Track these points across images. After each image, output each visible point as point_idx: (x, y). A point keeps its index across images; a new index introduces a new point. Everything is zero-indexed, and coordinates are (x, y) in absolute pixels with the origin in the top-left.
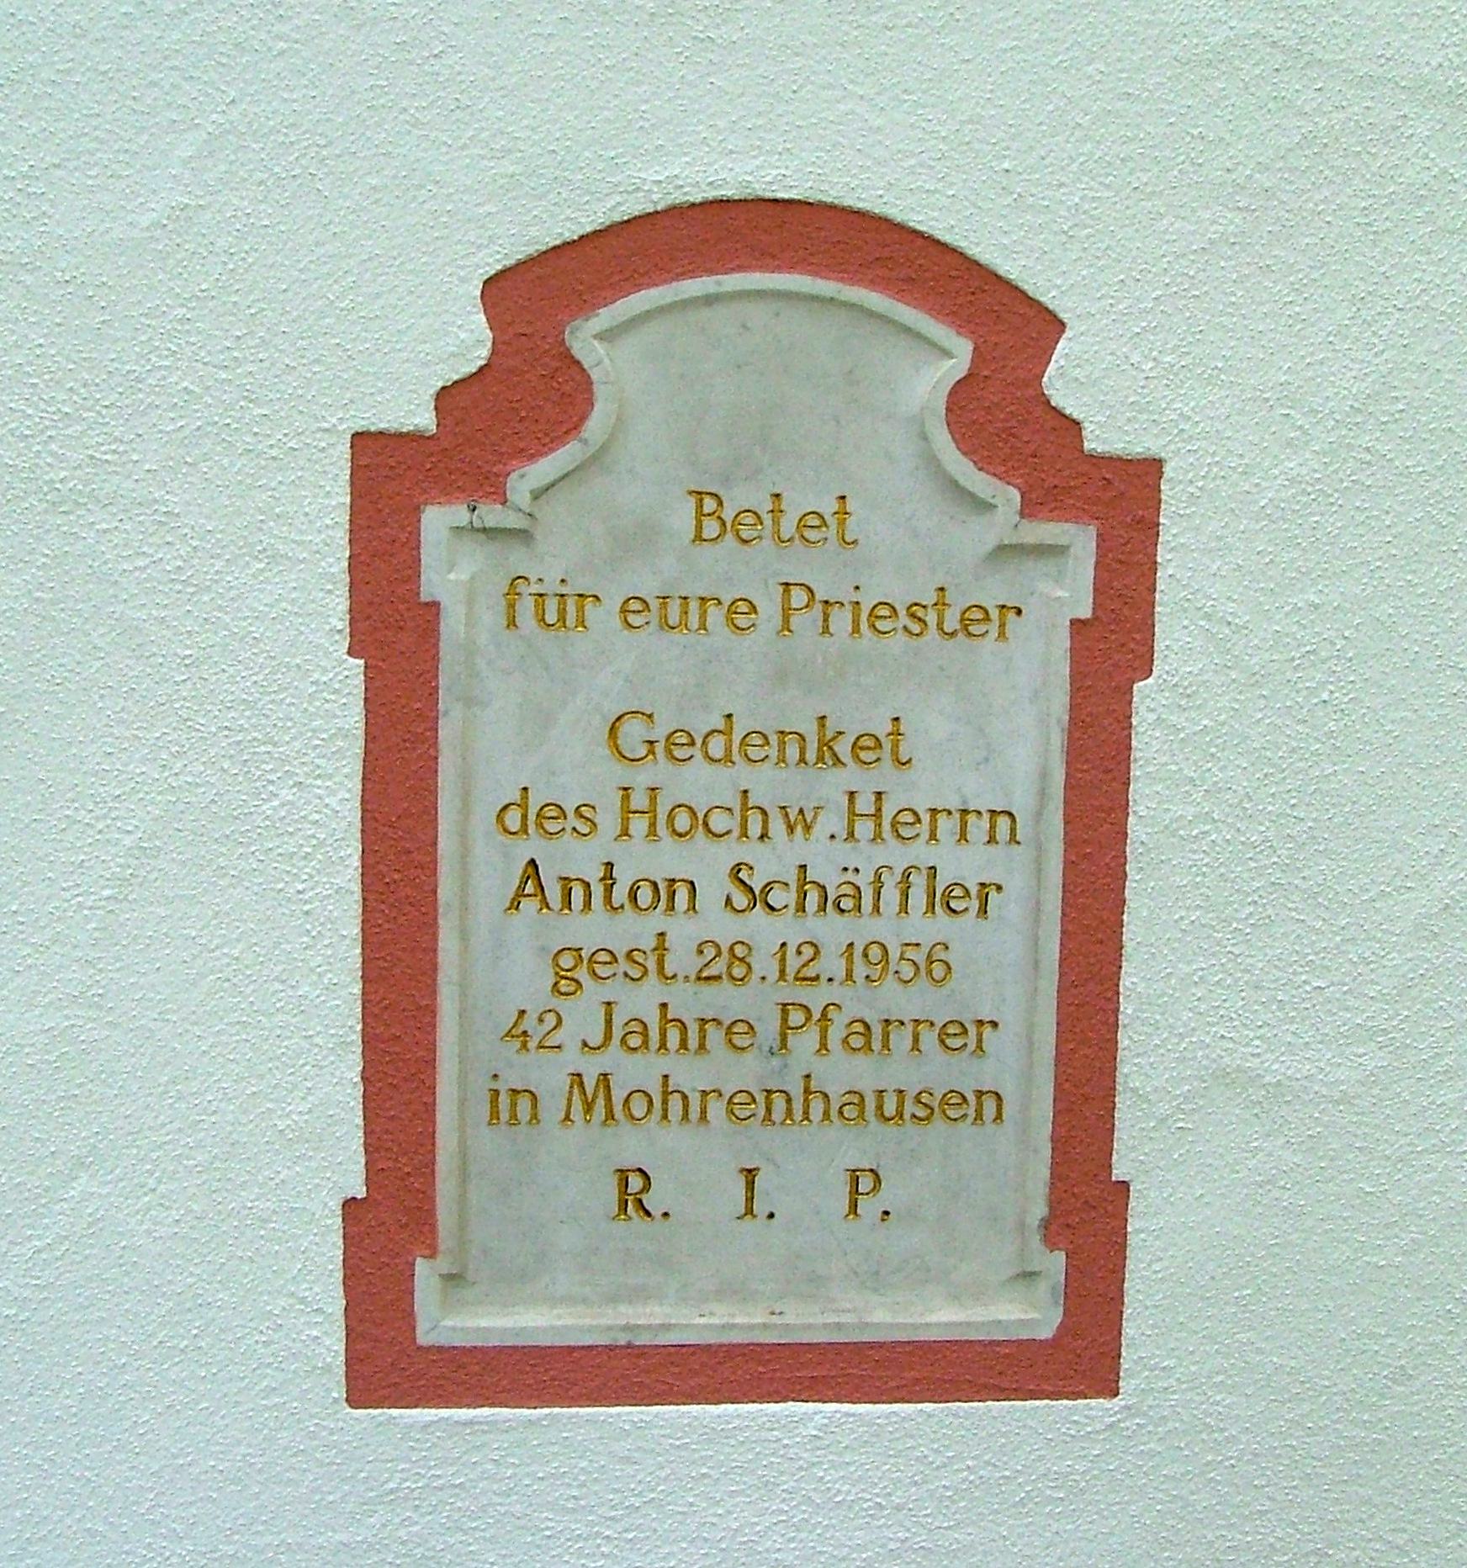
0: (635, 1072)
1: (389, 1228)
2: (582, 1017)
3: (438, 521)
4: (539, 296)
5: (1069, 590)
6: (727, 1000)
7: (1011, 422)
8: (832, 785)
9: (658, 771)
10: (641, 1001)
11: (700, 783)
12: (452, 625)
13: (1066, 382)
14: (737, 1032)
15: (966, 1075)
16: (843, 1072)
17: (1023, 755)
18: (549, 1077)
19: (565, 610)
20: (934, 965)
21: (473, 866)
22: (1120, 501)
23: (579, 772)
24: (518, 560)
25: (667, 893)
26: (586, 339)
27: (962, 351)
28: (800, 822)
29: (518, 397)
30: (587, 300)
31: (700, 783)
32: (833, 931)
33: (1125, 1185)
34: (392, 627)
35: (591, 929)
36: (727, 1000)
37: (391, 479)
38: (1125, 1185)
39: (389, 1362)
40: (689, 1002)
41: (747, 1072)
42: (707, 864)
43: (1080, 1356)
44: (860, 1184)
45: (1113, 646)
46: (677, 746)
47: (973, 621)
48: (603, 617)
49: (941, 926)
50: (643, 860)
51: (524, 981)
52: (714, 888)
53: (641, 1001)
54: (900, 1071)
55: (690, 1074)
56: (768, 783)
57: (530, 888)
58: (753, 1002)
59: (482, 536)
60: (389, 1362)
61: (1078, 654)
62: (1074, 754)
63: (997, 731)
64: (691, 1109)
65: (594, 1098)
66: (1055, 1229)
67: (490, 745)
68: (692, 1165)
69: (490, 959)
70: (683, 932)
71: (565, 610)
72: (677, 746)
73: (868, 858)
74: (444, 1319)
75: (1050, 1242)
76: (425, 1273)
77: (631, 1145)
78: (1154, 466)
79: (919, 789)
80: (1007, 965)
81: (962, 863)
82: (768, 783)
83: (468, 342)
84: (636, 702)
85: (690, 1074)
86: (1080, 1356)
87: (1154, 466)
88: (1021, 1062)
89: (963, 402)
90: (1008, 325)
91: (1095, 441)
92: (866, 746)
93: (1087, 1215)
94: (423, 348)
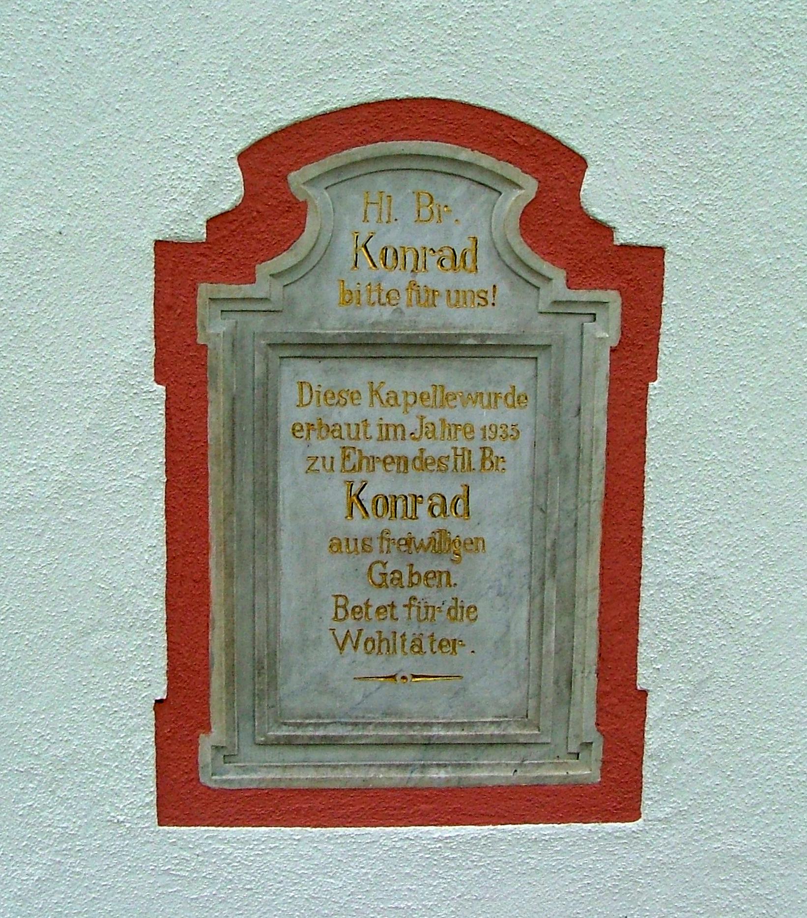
1: (179, 719)
4: (270, 159)
5: (606, 331)
26: (297, 180)
29: (258, 225)
33: (645, 693)
34: (179, 360)
35: (361, 427)
38: (645, 693)
39: (183, 798)
43: (616, 794)
59: (423, 747)
60: (183, 798)
74: (216, 774)
75: (158, 383)
78: (661, 250)
84: (351, 257)
86: (616, 794)
87: (661, 250)
89: (532, 222)
93: (622, 708)
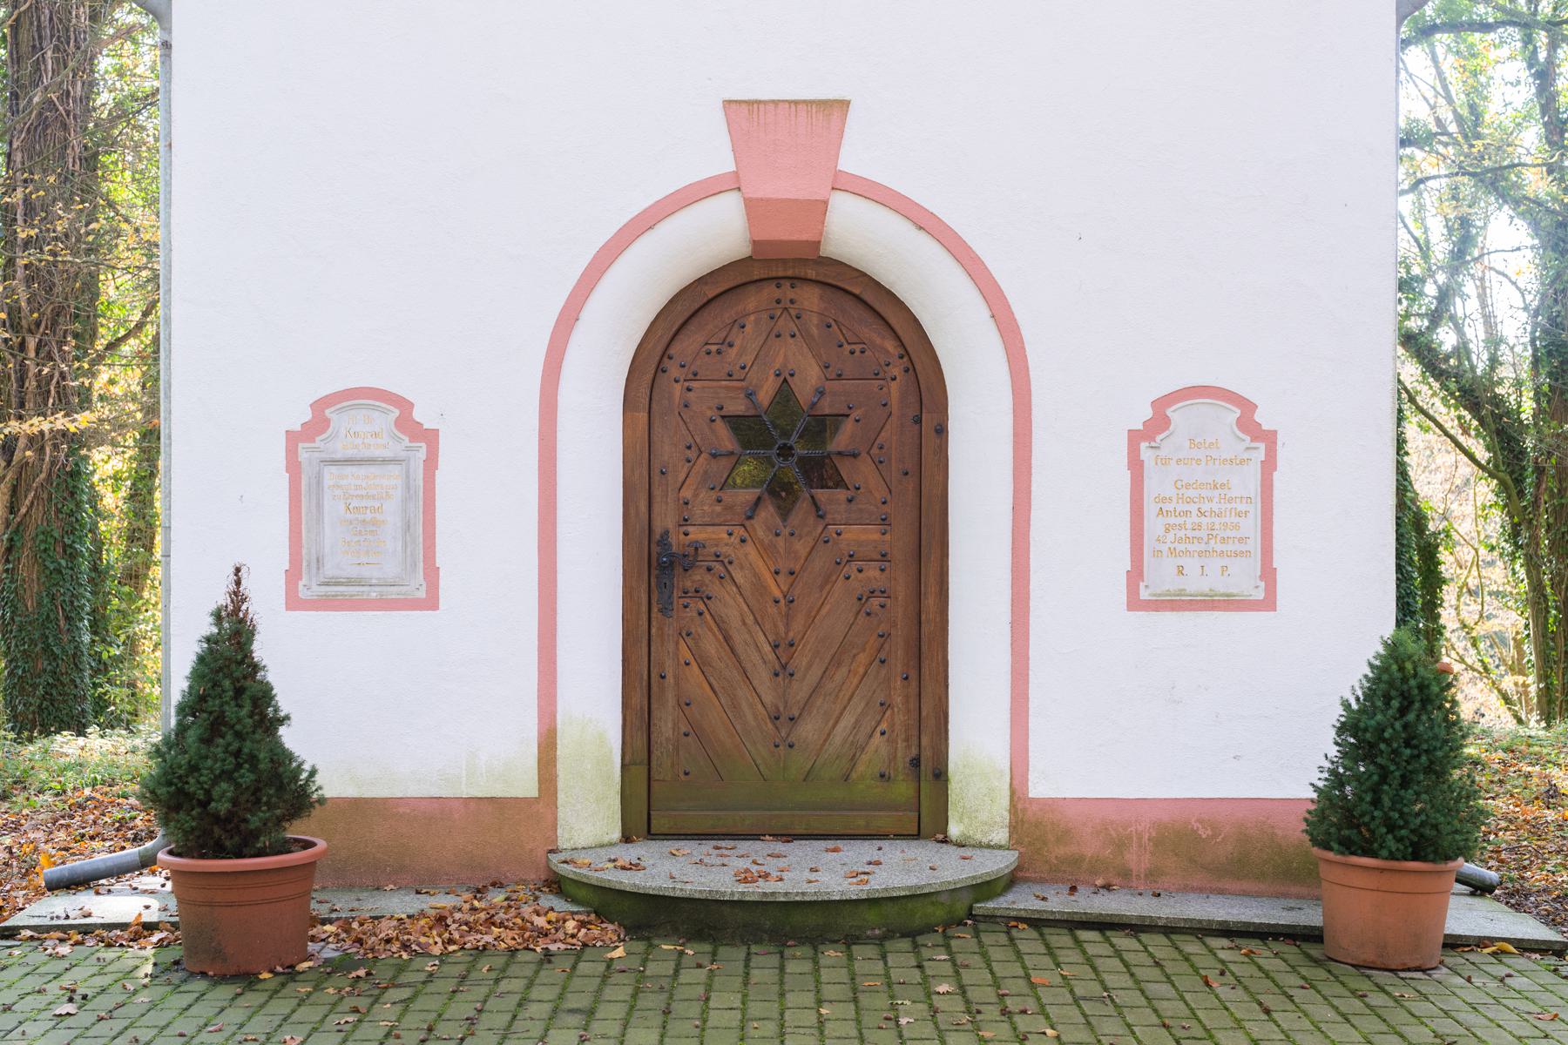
0: (1182, 547)
1: (1135, 575)
2: (1170, 537)
3: (1144, 445)
4: (1161, 405)
6: (1196, 533)
7: (1248, 425)
8: (1216, 492)
9: (1183, 491)
10: (1182, 534)
11: (1191, 493)
12: (1146, 465)
13: (1258, 417)
14: (1199, 539)
15: (1243, 548)
16: (1219, 547)
17: (1253, 487)
18: (1165, 548)
19: (1165, 461)
20: (1236, 527)
21: (1150, 509)
22: (1269, 439)
23: (1170, 492)
24: (1158, 452)
25: (1187, 513)
26: (1169, 412)
27: (1239, 412)
28: (1210, 500)
29: (1158, 424)
30: (1169, 405)
31: (1191, 493)
32: (1217, 520)
34: (1136, 466)
35: (1172, 520)
36: (1196, 533)
37: (1135, 438)
40: (1190, 534)
41: (1203, 547)
42: (1193, 508)
44: (1224, 568)
45: (1269, 465)
46: (1187, 486)
47: (1242, 462)
48: (1173, 463)
49: (1238, 519)
50: (1182, 507)
51: (1160, 531)
52: (1195, 512)
53: (1182, 534)
54: (1230, 547)
55: (1191, 547)
56: (1205, 493)
57: (1403, 74)
58: (1203, 534)
61: (1263, 468)
62: (1262, 486)
63: (1247, 482)
64: (1187, 553)
65: (1172, 552)
66: (1262, 577)
67: (1154, 485)
68: (1191, 565)
69: (1153, 525)
70: (1189, 521)
71: (1165, 461)
72: (1187, 486)
73: (1223, 507)
76: (1142, 585)
77: (1180, 562)
79: (1234, 493)
80: (1251, 526)
81: (1241, 507)
82: (1205, 493)
83: (1148, 413)
85: (1191, 547)
88: (1255, 545)
90: (1248, 407)
91: (1265, 427)
92: (1223, 485)
93: (1268, 574)
94: (1141, 414)
